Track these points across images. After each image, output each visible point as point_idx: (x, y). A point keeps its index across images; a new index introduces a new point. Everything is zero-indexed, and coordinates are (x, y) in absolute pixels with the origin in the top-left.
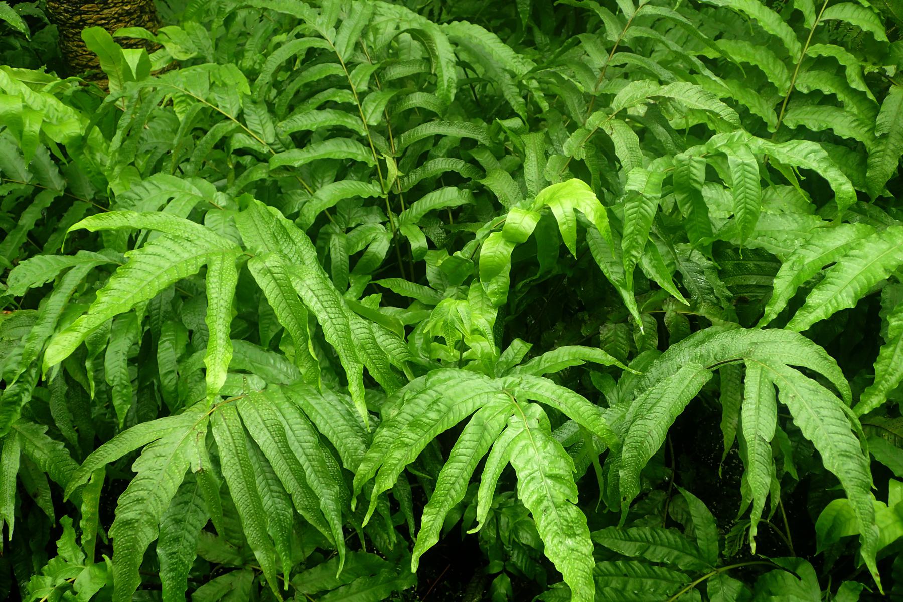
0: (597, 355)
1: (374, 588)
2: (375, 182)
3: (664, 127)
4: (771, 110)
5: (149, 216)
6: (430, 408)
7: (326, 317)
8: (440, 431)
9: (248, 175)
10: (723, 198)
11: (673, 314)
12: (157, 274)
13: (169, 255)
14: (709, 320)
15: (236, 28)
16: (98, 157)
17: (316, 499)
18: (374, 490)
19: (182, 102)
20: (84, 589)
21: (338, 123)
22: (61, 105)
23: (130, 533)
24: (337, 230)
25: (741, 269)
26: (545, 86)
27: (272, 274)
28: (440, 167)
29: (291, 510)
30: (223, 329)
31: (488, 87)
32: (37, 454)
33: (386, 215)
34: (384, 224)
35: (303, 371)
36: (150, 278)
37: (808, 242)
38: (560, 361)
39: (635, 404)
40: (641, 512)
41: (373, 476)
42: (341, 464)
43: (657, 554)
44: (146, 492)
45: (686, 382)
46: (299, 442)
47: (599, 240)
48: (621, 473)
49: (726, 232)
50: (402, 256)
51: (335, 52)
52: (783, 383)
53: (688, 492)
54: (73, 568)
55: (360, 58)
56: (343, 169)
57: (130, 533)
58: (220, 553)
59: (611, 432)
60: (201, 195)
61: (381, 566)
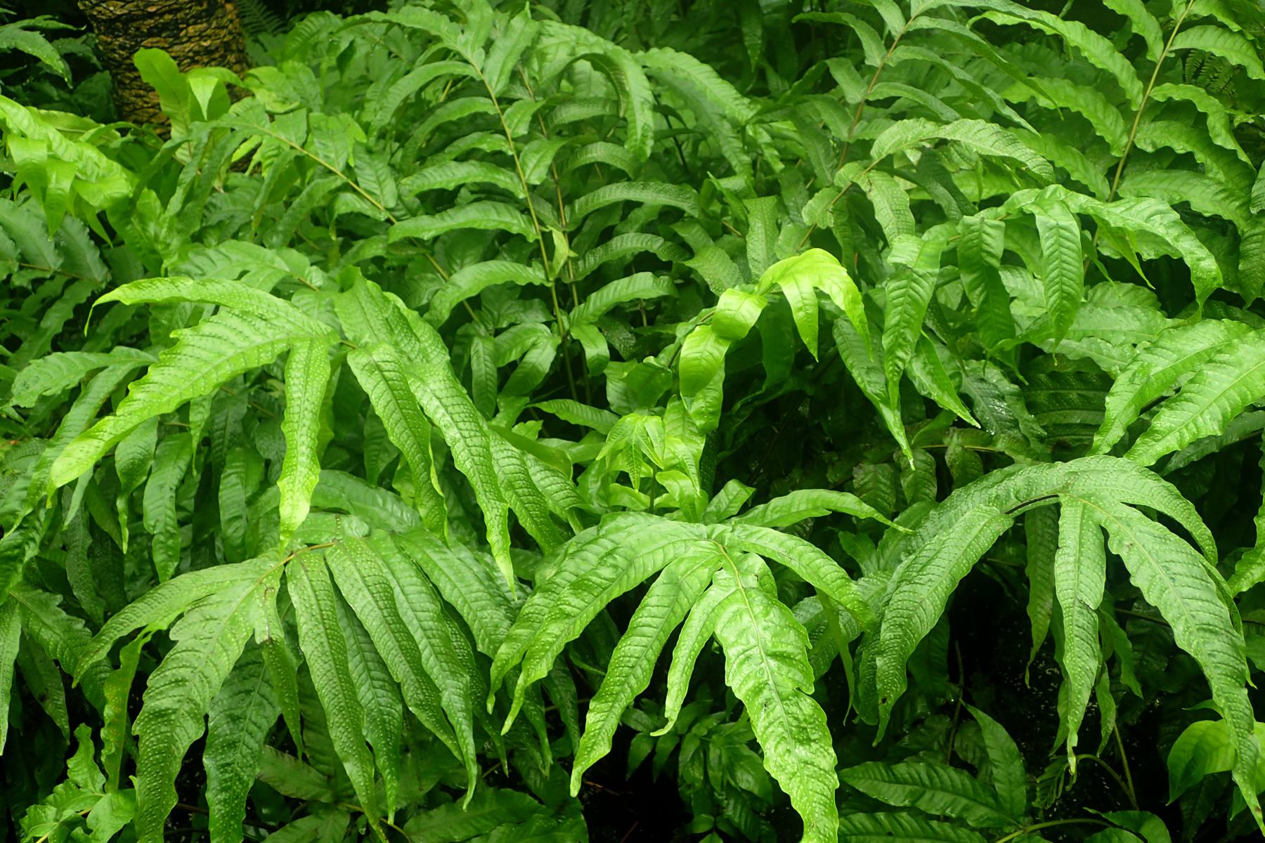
0: (848, 503)
3: (945, 187)
4: (1101, 177)
5: (209, 286)
6: (601, 562)
7: (458, 436)
8: (617, 593)
9: (357, 252)
10: (1031, 288)
11: (959, 449)
12: (216, 363)
14: (1010, 457)
15: (354, 71)
16: (152, 228)
17: (436, 691)
18: (520, 681)
20: (102, 825)
21: (486, 180)
22: (104, 159)
23: (163, 729)
24: (482, 330)
25: (1058, 401)
26: (781, 144)
27: (381, 371)
28: (629, 245)
29: (400, 707)
31: (701, 147)
32: (46, 635)
33: (552, 313)
34: (548, 324)
36: (205, 369)
37: (1155, 344)
39: (900, 569)
40: (915, 747)
42: (474, 645)
43: (936, 803)
44: (189, 670)
45: (975, 532)
47: (851, 337)
48: (879, 662)
49: (1037, 332)
50: (575, 378)
51: (482, 82)
52: (1113, 521)
53: (981, 713)
54: (90, 797)
55: (518, 92)
56: (501, 243)
57: (163, 729)
58: (296, 780)
59: (865, 604)
60: (287, 269)
61: (534, 811)
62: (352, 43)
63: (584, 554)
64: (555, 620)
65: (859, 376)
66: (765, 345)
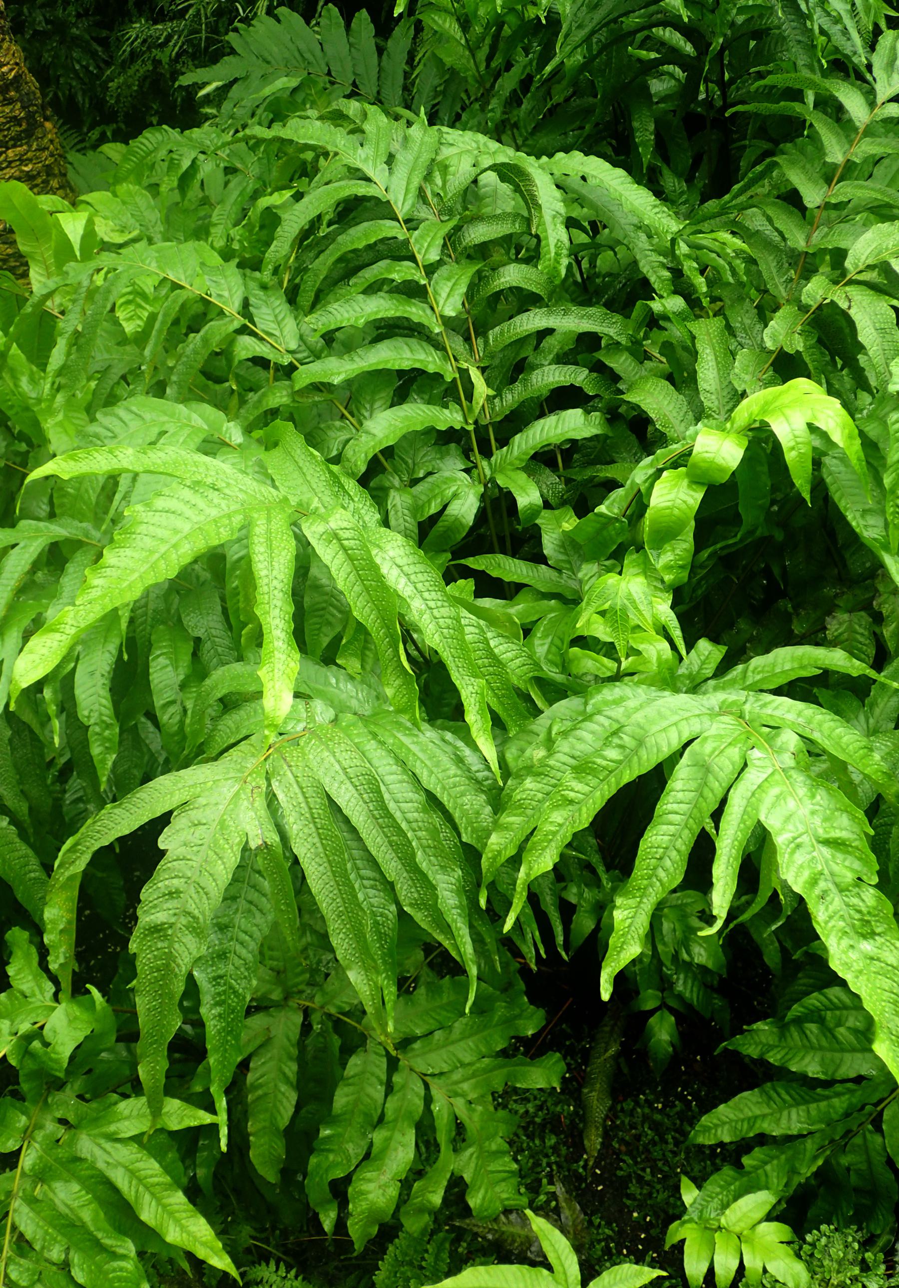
1: (485, 1033)
2: (453, 406)
7: (423, 607)
9: (259, 401)
12: (173, 542)
13: (189, 512)
18: (522, 874)
19: (128, 302)
20: (60, 1038)
21: (398, 314)
23: (160, 945)
24: (396, 482)
27: (339, 540)
28: (551, 379)
29: (393, 908)
30: (282, 624)
34: (467, 471)
35: (389, 692)
36: (163, 549)
38: (778, 670)
41: (513, 852)
42: (459, 835)
44: (182, 880)
46: (397, 802)
51: (388, 202)
56: (406, 385)
57: (160, 945)
62: (194, 161)
63: (578, 733)
64: (556, 807)
65: (854, 519)
66: (741, 489)
